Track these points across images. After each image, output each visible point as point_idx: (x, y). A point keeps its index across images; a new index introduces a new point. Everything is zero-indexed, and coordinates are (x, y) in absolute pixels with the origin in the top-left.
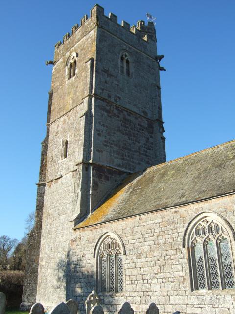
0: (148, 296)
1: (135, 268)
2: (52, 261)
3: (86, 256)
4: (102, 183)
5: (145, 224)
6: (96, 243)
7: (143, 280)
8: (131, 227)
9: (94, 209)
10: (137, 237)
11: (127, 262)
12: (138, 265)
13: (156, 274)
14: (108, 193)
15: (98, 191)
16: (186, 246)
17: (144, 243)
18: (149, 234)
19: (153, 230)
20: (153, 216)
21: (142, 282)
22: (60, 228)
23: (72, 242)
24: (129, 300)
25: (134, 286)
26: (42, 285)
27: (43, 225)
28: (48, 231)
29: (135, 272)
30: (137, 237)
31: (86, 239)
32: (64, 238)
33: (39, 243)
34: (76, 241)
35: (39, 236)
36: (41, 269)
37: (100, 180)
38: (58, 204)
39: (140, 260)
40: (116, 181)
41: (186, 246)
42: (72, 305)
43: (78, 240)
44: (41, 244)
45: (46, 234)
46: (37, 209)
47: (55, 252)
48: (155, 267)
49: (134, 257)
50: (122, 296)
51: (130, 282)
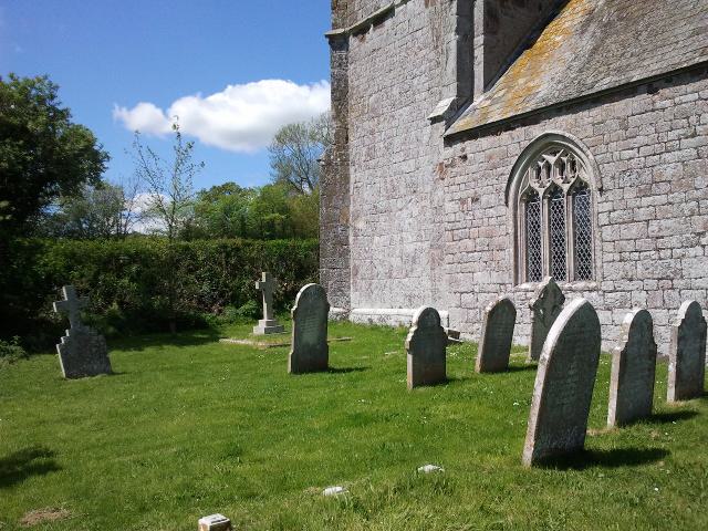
0: (672, 288)
1: (633, 221)
2: (382, 219)
3: (484, 199)
4: (506, 14)
5: (667, 103)
6: (510, 167)
7: (658, 250)
8: (622, 115)
9: (488, 84)
10: (641, 140)
11: (608, 206)
12: (642, 214)
13: (699, 234)
14: (524, 40)
15: (500, 36)
16: (511, 203)
17: (663, 156)
18: (681, 132)
19: (693, 119)
20: (367, 194)
21: (656, 256)
22: (397, 141)
23: (441, 170)
24: (595, 299)
25: (628, 266)
26: (361, 271)
27: (351, 138)
28: (365, 149)
29: (634, 230)
30: (641, 140)
31: (481, 157)
32: (412, 162)
33: (346, 178)
34: (452, 165)
35: (345, 162)
36: (356, 235)
37: (502, 5)
38: (388, 83)
39: (646, 201)
40: (540, 9)
41: (511, 203)
42: (503, 312)
43: (458, 161)
44: (352, 181)
45: (363, 158)
46: (334, 99)
47: (388, 198)
48: (696, 217)
49: (630, 194)
50: (590, 291)
51: (617, 257)
